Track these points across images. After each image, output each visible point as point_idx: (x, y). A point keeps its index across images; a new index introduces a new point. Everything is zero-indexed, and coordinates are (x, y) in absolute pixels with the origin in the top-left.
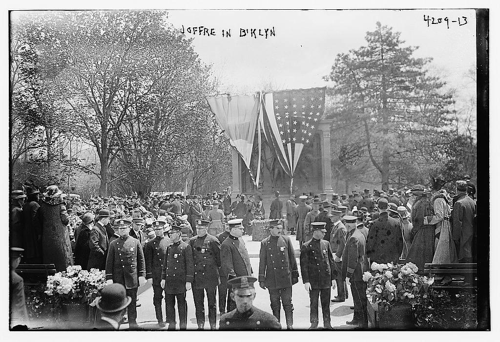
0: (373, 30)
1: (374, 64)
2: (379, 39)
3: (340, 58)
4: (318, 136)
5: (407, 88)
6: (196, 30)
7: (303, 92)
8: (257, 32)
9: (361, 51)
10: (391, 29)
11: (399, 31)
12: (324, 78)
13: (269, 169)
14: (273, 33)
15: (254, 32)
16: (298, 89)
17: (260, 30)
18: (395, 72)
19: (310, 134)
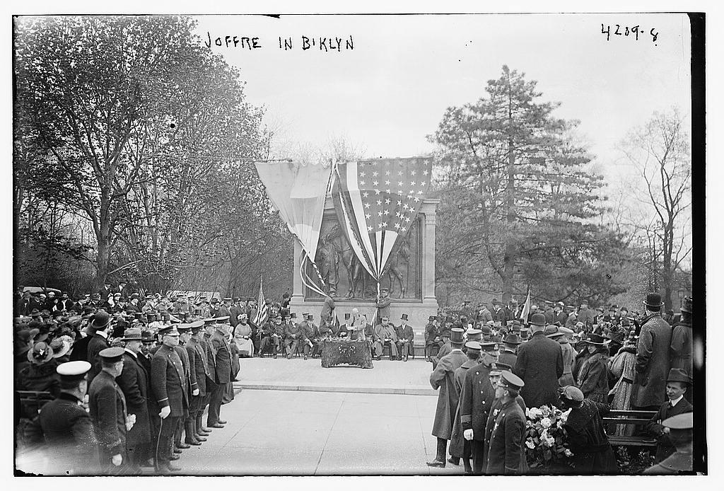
0: (497, 78)
1: (498, 125)
2: (505, 89)
3: (451, 114)
4: (419, 221)
5: (542, 162)
6: (230, 41)
7: (401, 163)
8: (327, 43)
9: (480, 106)
10: (523, 75)
11: (534, 79)
12: (427, 137)
13: (346, 266)
14: (350, 45)
15: (323, 43)
16: (394, 157)
17: (330, 40)
18: (525, 137)
19: (408, 220)
